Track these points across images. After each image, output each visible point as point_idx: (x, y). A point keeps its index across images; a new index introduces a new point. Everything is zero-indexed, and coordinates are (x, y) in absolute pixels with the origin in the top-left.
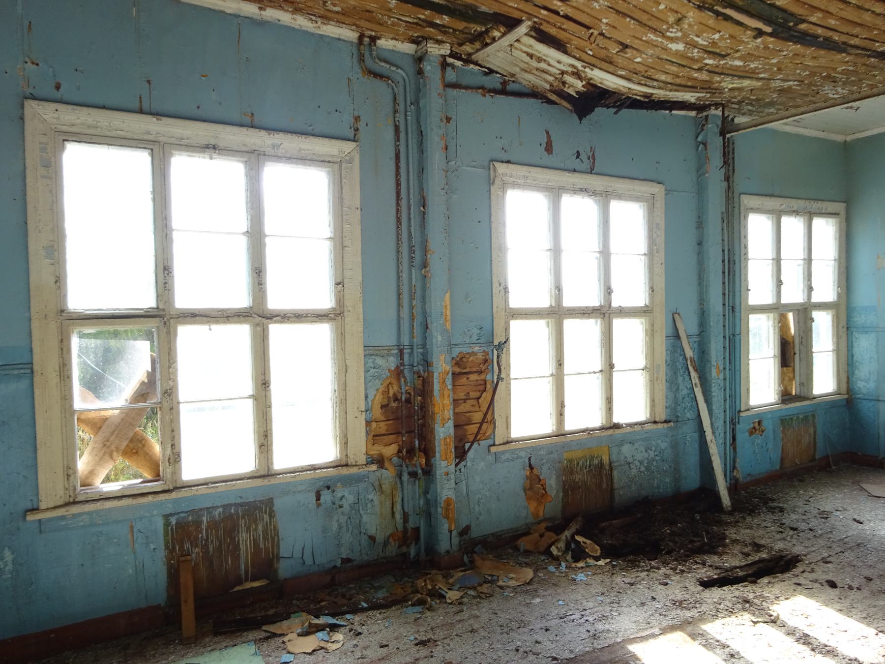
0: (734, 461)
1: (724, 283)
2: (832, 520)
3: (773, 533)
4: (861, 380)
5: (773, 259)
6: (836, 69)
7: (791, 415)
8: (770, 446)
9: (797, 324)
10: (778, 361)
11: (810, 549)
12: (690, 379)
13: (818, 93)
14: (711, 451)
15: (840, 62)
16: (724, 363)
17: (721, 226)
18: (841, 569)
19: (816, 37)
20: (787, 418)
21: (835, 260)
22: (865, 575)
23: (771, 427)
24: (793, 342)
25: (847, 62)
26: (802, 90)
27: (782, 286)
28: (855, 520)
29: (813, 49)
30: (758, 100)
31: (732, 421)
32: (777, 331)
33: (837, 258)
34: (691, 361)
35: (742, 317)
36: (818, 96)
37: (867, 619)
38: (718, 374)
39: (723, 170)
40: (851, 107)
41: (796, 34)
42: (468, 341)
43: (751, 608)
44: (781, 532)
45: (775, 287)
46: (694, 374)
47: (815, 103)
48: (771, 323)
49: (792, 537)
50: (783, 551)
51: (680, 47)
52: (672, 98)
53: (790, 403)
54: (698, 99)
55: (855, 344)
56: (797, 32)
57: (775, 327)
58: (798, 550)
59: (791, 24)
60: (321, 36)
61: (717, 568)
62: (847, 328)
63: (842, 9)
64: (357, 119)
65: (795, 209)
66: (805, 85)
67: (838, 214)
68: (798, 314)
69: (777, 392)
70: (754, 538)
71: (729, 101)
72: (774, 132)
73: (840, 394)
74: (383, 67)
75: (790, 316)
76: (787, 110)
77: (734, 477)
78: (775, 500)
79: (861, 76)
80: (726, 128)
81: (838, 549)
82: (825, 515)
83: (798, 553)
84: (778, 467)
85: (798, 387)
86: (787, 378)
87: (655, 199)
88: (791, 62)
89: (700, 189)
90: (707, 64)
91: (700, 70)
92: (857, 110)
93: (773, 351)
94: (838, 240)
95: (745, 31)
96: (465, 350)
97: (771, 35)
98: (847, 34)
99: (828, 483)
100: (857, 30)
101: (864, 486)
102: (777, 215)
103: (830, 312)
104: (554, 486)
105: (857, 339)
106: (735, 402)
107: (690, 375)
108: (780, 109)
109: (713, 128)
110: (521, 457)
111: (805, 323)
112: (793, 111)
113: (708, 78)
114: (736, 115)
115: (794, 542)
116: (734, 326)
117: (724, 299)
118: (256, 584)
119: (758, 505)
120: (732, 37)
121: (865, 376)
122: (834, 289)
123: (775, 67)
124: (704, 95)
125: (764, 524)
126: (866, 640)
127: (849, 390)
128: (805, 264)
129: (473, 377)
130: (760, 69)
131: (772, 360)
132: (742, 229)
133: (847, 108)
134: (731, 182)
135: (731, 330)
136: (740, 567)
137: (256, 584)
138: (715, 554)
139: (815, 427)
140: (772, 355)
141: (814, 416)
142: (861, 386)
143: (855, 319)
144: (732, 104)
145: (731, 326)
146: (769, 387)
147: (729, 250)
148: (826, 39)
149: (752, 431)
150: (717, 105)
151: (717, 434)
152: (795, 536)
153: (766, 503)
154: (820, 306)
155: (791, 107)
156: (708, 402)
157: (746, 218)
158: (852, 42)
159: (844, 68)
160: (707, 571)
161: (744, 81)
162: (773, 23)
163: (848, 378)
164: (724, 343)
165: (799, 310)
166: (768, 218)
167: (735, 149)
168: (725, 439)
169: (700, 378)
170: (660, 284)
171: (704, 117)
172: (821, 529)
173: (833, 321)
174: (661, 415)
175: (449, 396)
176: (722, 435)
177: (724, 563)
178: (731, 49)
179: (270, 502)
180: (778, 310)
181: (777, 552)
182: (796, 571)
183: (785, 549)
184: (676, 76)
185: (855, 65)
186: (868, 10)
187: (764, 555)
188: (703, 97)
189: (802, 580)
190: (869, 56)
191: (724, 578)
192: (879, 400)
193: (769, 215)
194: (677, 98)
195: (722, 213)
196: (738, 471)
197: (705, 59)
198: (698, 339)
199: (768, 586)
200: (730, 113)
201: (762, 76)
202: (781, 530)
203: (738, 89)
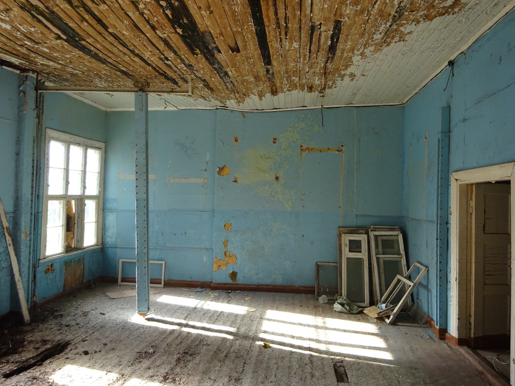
0: (34, 291)
1: (33, 180)
2: (89, 316)
3: (56, 331)
4: (108, 237)
5: (64, 169)
6: (101, 71)
7: (70, 259)
8: (58, 279)
9: (77, 207)
10: (64, 228)
11: (76, 336)
12: (6, 241)
13: (92, 82)
14: (18, 287)
15: (104, 69)
16: (31, 231)
17: (32, 145)
18: (92, 343)
19: (91, 51)
20: (68, 261)
21: (98, 173)
22: (103, 343)
23: (58, 267)
24: (74, 217)
25: (107, 70)
26: (84, 77)
27: (69, 185)
28: (101, 313)
29: (89, 57)
30: (58, 75)
31: (34, 266)
32: (64, 211)
33: (99, 172)
34: (7, 230)
35: (44, 201)
36: (92, 83)
37: (102, 367)
38: (26, 237)
39: (36, 111)
40: (109, 94)
41: (80, 45)
43: (37, 382)
44: (60, 329)
45: (65, 185)
46: (8, 238)
47: (91, 86)
48: (61, 206)
49: (66, 331)
50: (60, 341)
51: (8, 27)
52: (2, 58)
53: (71, 252)
54: (20, 63)
55: (106, 218)
56: (80, 44)
57: (64, 208)
58: (69, 337)
59: (77, 39)
61: (17, 362)
62: (103, 210)
63: (103, 41)
65: (78, 142)
66: (86, 75)
67: (101, 149)
68: (78, 201)
69: (64, 246)
70: (43, 337)
71: (41, 71)
72: (69, 97)
73: (98, 245)
75: (73, 202)
76: (76, 86)
77: (33, 301)
78: (58, 311)
79: (114, 79)
80: (39, 86)
81: (91, 332)
82: (85, 314)
83: (69, 340)
84: (62, 291)
85: (76, 242)
86: (70, 238)
88: (77, 60)
89: (20, 120)
90: (26, 44)
91: (21, 46)
92: (112, 96)
93: (62, 222)
94: (100, 162)
95: (50, 33)
97: (66, 41)
98: (106, 55)
99: (89, 295)
100: (110, 55)
101: (107, 294)
102: (68, 144)
103: (95, 201)
105: (107, 215)
106: (37, 254)
107: (6, 239)
108: (72, 85)
109: (30, 85)
111: (81, 206)
112: (78, 87)
113: (27, 53)
114: (46, 80)
115: (67, 333)
116: (38, 207)
117: (32, 190)
119: (48, 316)
120: (42, 33)
121: (111, 235)
122: (97, 189)
123: (68, 60)
124: (24, 62)
125: (51, 327)
126: (101, 379)
127: (103, 243)
128: (82, 173)
130: (59, 58)
131: (61, 227)
132: (46, 148)
133: (107, 94)
134: (40, 120)
135: (36, 209)
136: (33, 358)
138: (16, 353)
139: (84, 265)
140: (61, 224)
141: (83, 259)
142: (109, 241)
143: (107, 205)
144: (44, 73)
145: (36, 207)
146: (59, 243)
147: (37, 160)
148: (96, 54)
149: (47, 271)
150: (34, 71)
151: (23, 275)
152: (68, 330)
153: (52, 313)
154: (90, 197)
155: (78, 85)
156: (18, 255)
157: (49, 142)
158: (109, 60)
159: (105, 72)
160: (9, 366)
161: (50, 62)
162: (67, 34)
163: (102, 236)
164: (31, 218)
165: (78, 199)
166: (63, 144)
167: (44, 100)
168: (29, 278)
169: (13, 240)
171: (25, 76)
172: (83, 323)
173: (96, 206)
176: (27, 276)
177: (22, 358)
178: (42, 40)
180: (66, 198)
181: (57, 342)
182: (67, 351)
183: (62, 339)
184: (5, 44)
185: (110, 72)
186: (116, 47)
187: (48, 346)
188: (24, 63)
189: (70, 355)
190: (117, 70)
191: (21, 367)
192: (116, 247)
193: (63, 143)
194: (6, 59)
195: (34, 137)
196: (36, 297)
197: (25, 40)
198: (13, 215)
199: (49, 365)
200: (42, 78)
201: (61, 62)
202: (60, 328)
203: (47, 65)
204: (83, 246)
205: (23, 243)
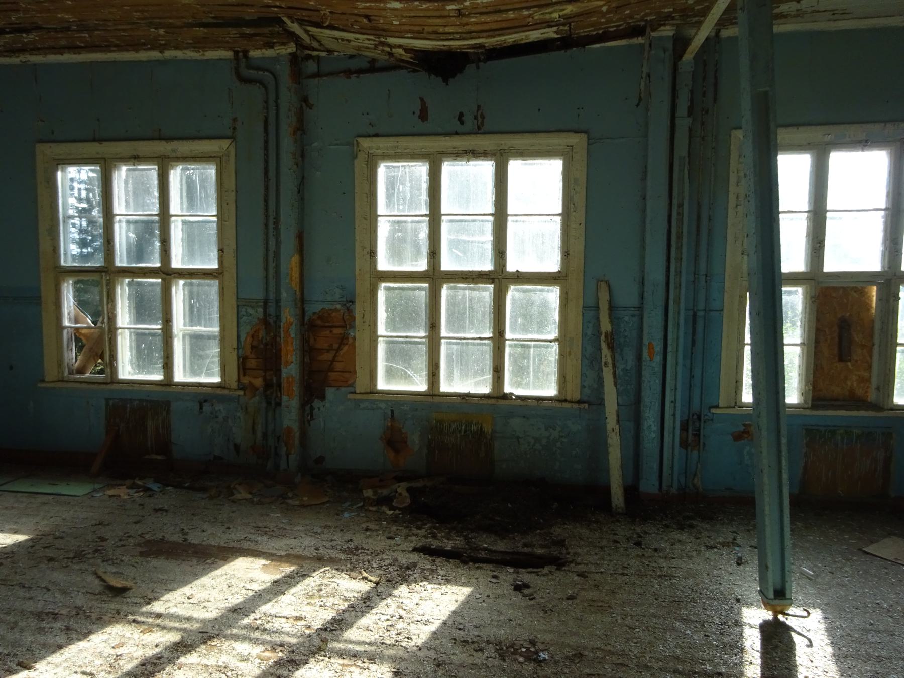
34: (605, 337)
42: (329, 299)
60: (207, 60)
64: (235, 120)
74: (253, 73)
87: (574, 150)
96: (327, 307)
104: (417, 442)
110: (381, 408)
118: (159, 457)
129: (337, 331)
137: (159, 457)
170: (578, 247)
174: (574, 393)
175: (292, 343)
179: (168, 404)
204: (173, 380)
205: (645, 365)
